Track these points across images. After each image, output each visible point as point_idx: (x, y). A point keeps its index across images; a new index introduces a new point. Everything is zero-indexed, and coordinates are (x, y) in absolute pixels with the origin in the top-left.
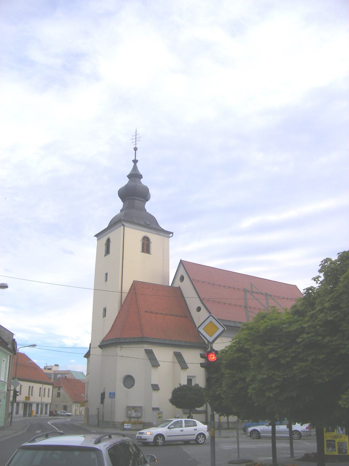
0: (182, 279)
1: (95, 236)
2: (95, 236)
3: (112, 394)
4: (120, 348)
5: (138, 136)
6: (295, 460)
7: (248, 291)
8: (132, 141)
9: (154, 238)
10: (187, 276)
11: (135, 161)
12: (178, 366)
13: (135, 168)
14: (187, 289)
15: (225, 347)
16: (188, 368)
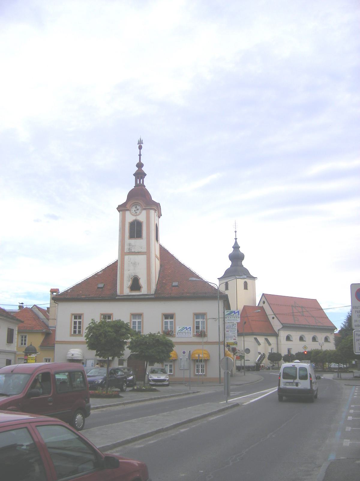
0: (264, 302)
6: (22, 322)
7: (294, 306)
9: (249, 281)
10: (267, 302)
11: (236, 239)
12: (267, 345)
13: (236, 243)
14: (268, 311)
15: (138, 144)
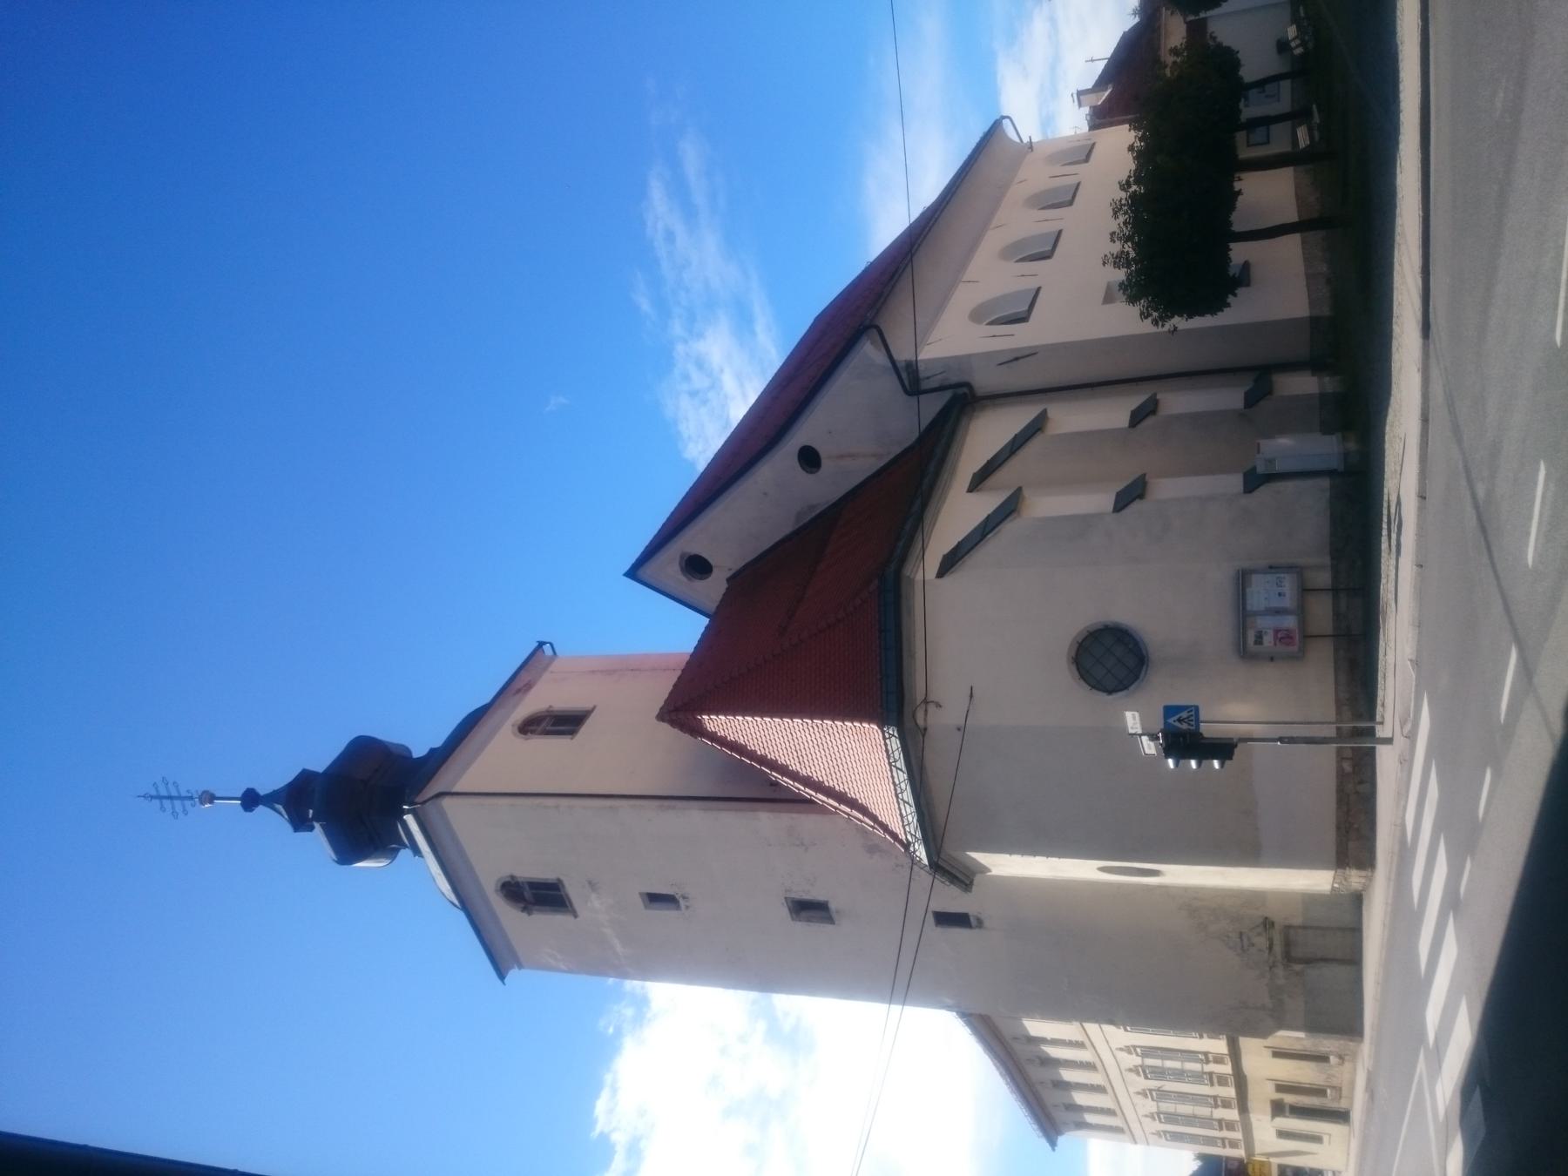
1: (502, 976)
2: (502, 976)
3: (1171, 721)
4: (931, 708)
5: (163, 792)
8: (181, 815)
13: (270, 800)
16: (1145, 475)
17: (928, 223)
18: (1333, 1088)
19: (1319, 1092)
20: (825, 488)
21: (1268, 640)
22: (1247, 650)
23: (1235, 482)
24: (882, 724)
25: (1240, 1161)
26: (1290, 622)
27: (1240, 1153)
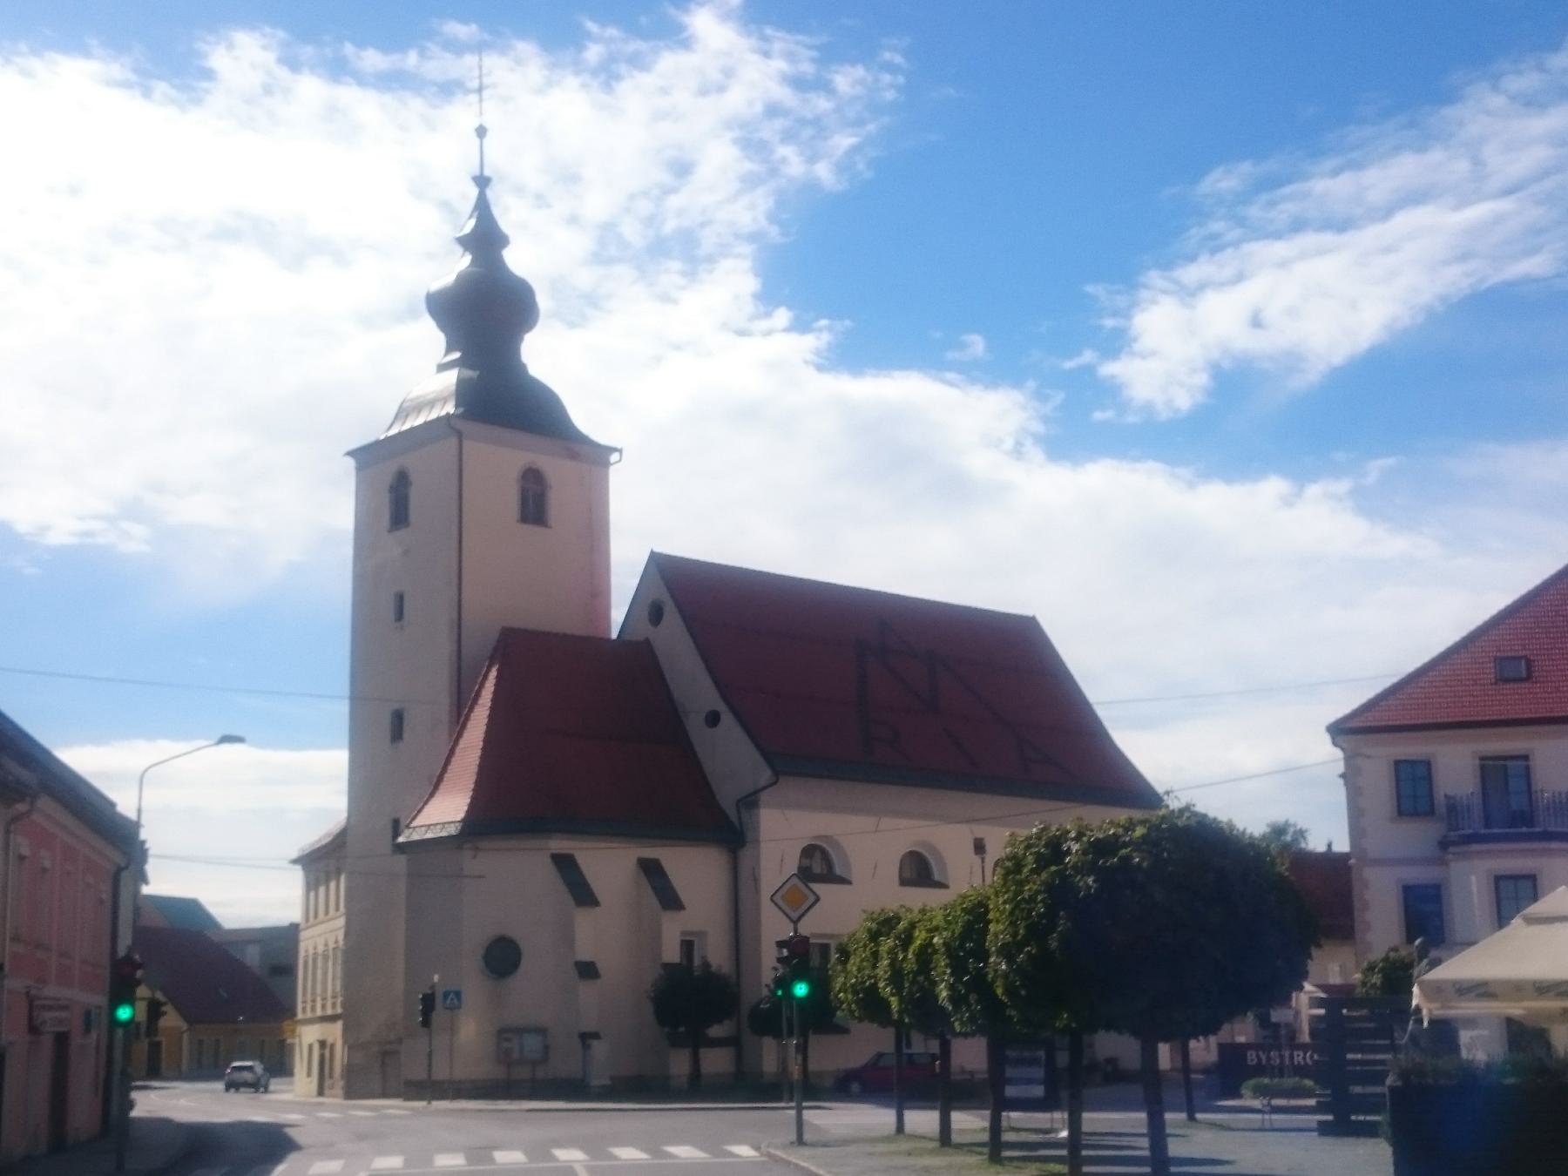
17: (110, 1062)
18: (333, 1084)
19: (331, 1077)
20: (695, 725)
21: (506, 1045)
22: (505, 1033)
23: (588, 1026)
24: (465, 821)
25: (295, 1015)
26: (515, 1055)
27: (300, 1016)
